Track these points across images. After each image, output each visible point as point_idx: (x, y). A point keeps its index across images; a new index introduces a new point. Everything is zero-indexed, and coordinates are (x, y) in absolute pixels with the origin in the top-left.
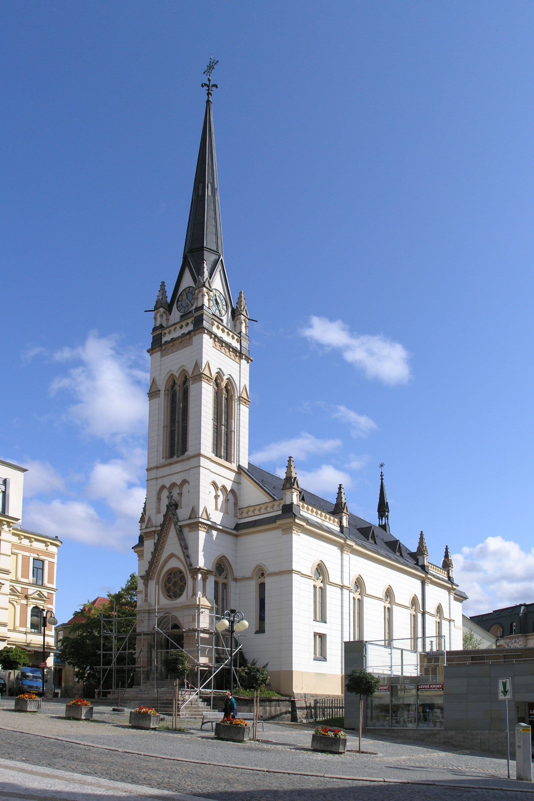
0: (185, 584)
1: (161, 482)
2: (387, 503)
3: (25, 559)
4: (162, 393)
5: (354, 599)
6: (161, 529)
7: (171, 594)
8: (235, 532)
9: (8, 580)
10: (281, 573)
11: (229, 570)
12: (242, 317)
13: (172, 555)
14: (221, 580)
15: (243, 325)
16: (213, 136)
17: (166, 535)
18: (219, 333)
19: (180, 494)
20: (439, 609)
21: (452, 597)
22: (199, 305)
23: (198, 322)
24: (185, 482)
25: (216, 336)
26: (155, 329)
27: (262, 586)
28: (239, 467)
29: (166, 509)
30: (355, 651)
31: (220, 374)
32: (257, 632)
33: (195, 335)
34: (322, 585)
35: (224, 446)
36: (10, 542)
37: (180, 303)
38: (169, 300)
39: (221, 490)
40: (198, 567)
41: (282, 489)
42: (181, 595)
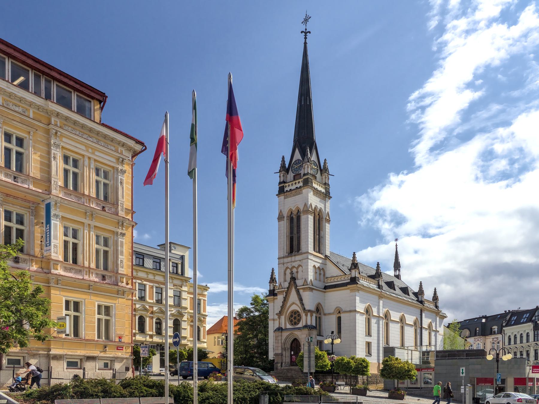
4: (285, 218)
8: (324, 290)
10: (350, 311)
13: (293, 303)
14: (318, 315)
17: (290, 293)
19: (297, 272)
24: (299, 266)
26: (280, 183)
27: (339, 319)
30: (389, 351)
42: (298, 324)
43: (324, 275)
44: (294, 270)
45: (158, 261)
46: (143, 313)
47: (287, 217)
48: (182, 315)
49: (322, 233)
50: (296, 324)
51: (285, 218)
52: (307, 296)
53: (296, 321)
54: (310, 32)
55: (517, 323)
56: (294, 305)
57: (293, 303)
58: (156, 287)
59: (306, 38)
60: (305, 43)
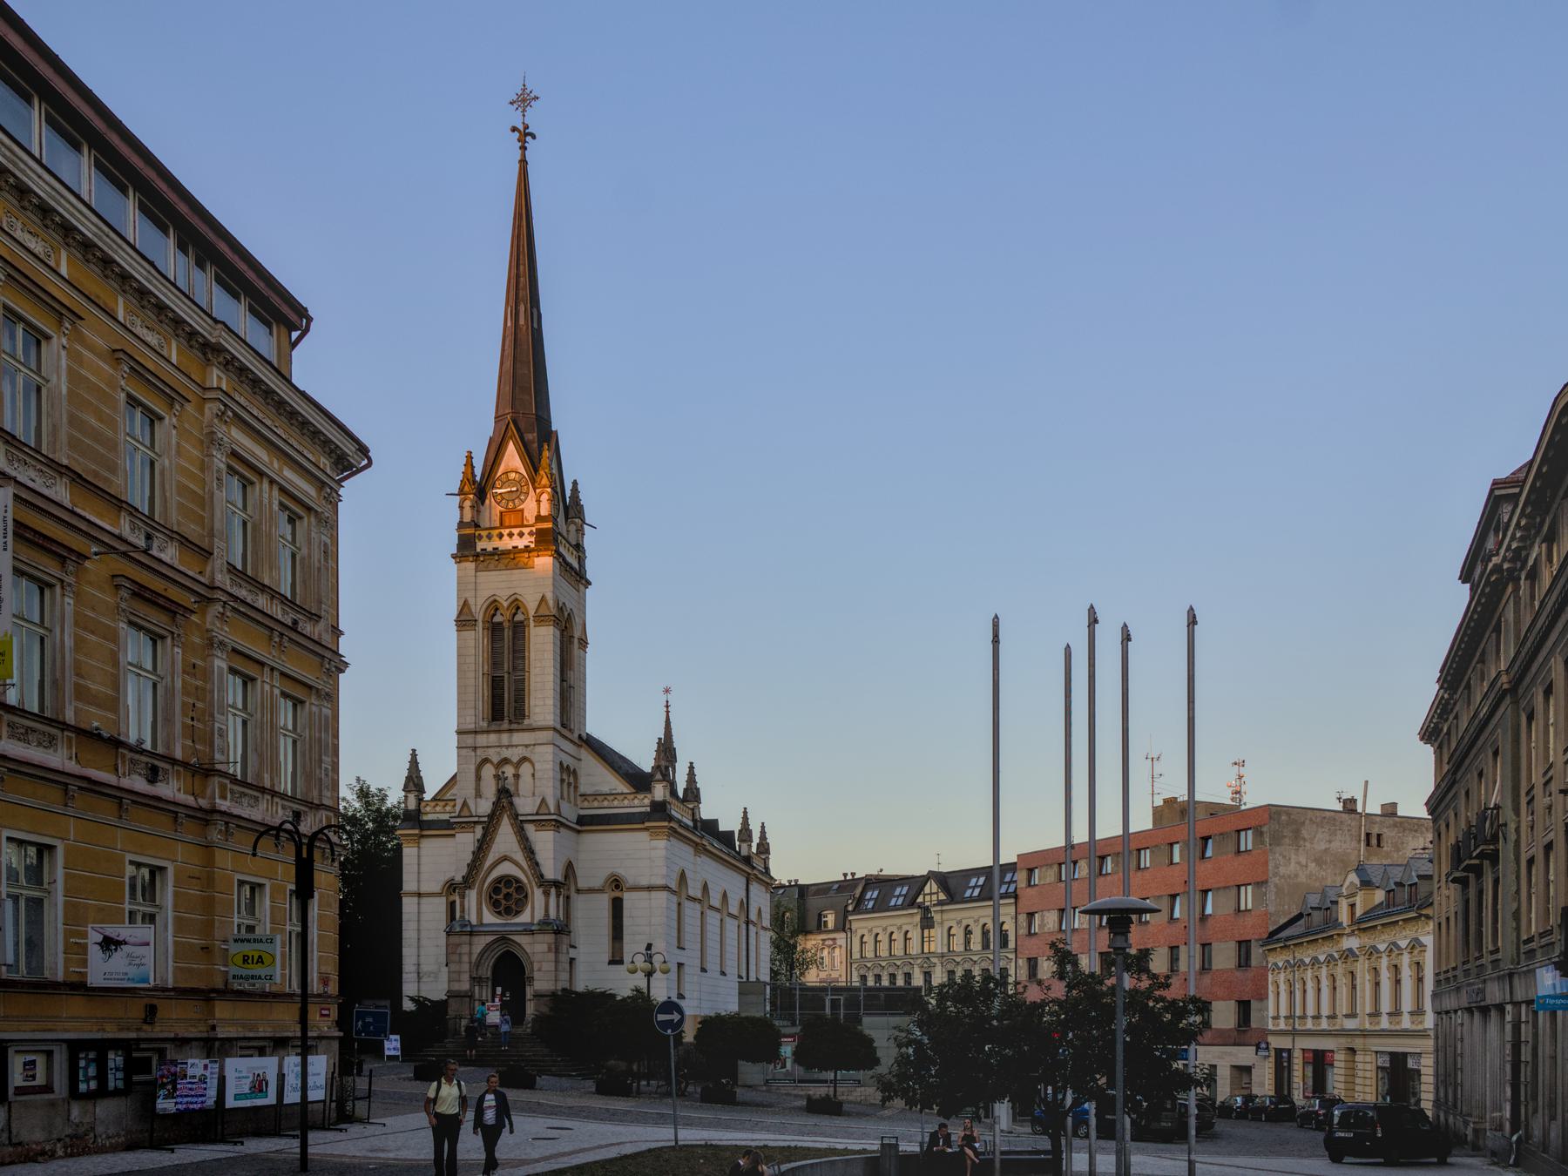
1: (481, 754)
4: (480, 624)
13: (505, 858)
17: (496, 830)
19: (517, 776)
27: (617, 906)
32: (611, 963)
43: (576, 788)
44: (509, 771)
49: (571, 675)
52: (544, 841)
54: (534, 137)
55: (881, 906)
56: (506, 864)
57: (505, 858)
59: (523, 148)
60: (523, 162)
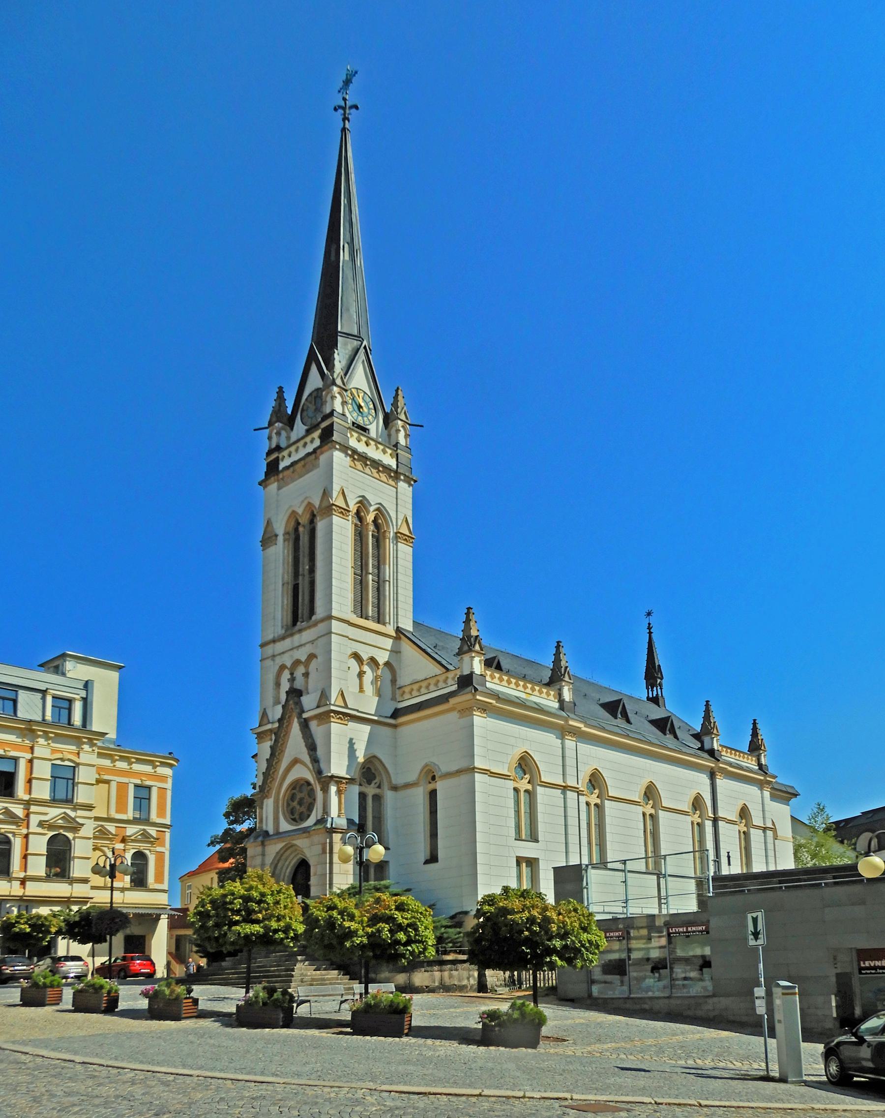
0: (314, 800)
2: (659, 666)
3: (122, 787)
4: (281, 538)
5: (588, 804)
6: (279, 727)
7: (296, 816)
9: (90, 818)
11: (384, 776)
12: (400, 422)
13: (296, 761)
15: (402, 434)
16: (352, 177)
17: (287, 733)
18: (361, 447)
19: (306, 675)
20: (744, 813)
21: (767, 794)
22: (328, 411)
23: (327, 435)
24: (312, 656)
25: (355, 451)
26: (269, 453)
27: (433, 794)
28: (398, 630)
29: (285, 697)
31: (363, 503)
32: (427, 862)
33: (322, 453)
34: (529, 787)
35: (371, 600)
36: (94, 766)
37: (305, 414)
38: (289, 411)
39: (368, 664)
40: (329, 775)
41: (458, 654)
42: (309, 816)
45: (11, 695)
46: (142, 847)
47: (286, 533)
48: (76, 827)
50: (304, 817)
51: (281, 538)
53: (303, 809)
56: (298, 766)
57: (296, 761)
58: (136, 786)
